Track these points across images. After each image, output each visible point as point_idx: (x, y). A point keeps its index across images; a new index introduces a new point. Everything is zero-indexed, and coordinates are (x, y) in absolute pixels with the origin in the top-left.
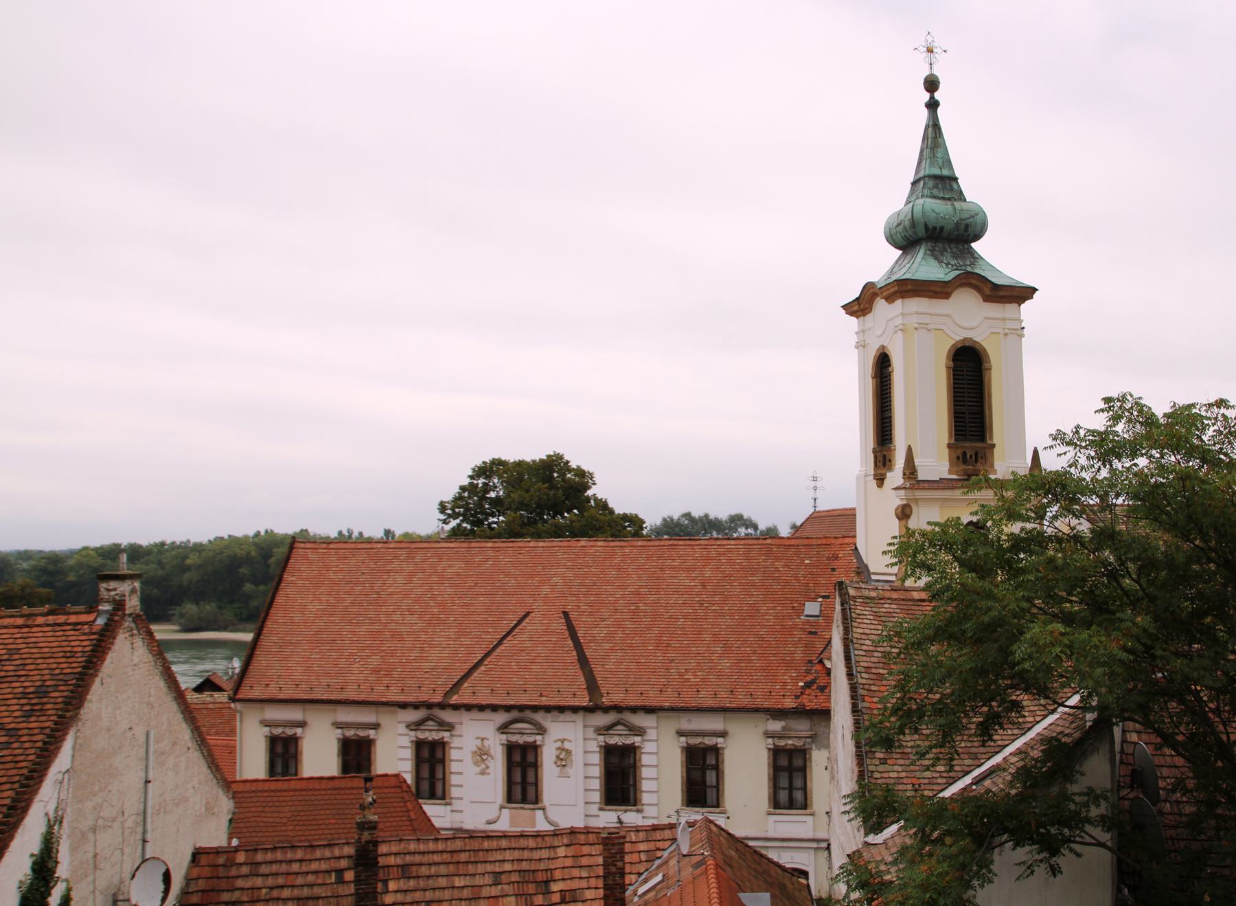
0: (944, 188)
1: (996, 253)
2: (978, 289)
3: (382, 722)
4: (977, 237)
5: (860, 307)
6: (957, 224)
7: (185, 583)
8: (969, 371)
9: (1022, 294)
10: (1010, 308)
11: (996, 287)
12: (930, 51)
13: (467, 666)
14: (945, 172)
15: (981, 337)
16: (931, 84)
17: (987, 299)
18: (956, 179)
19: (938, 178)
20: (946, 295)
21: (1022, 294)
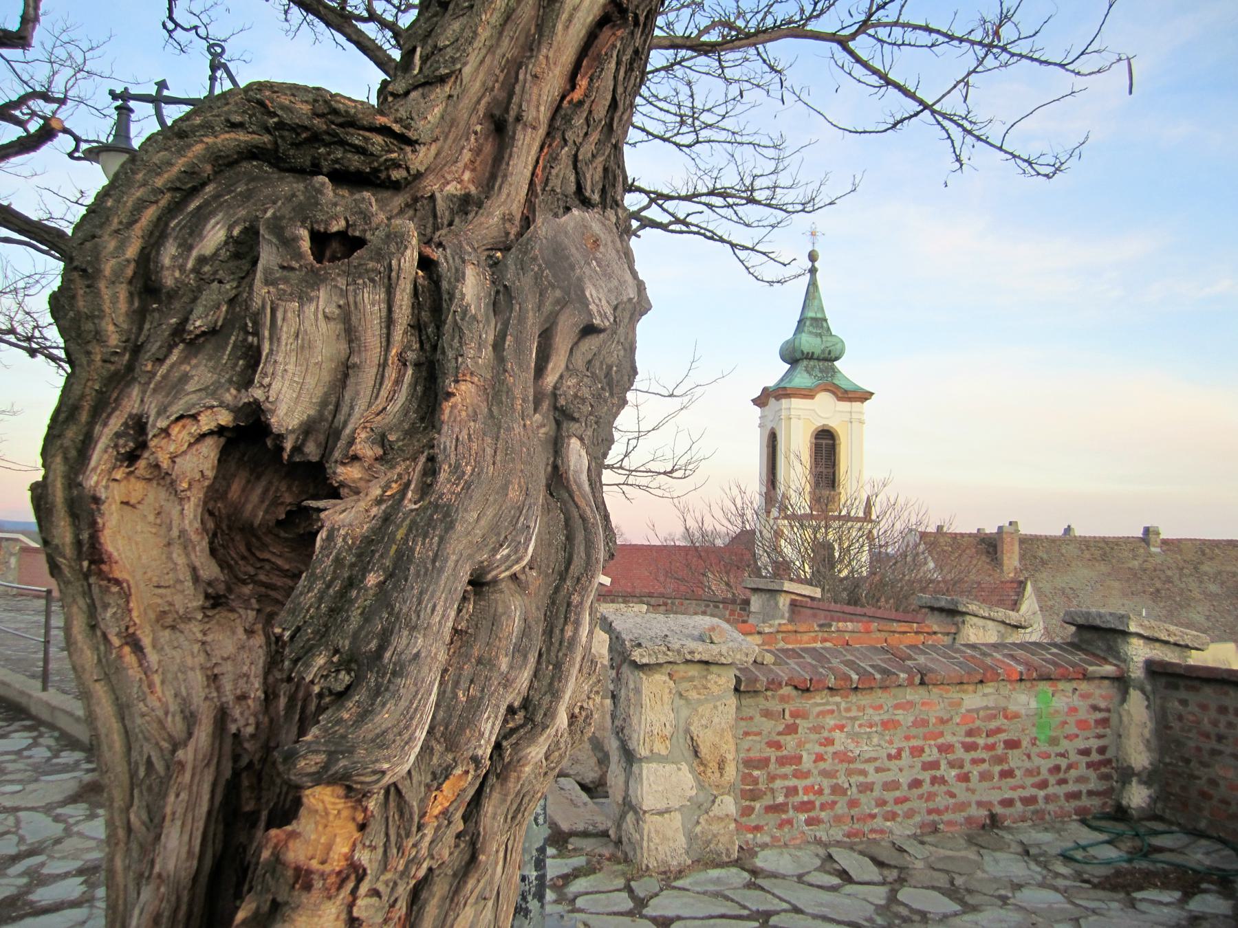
0: (817, 327)
1: (849, 369)
2: (834, 393)
3: (311, 119)
4: (837, 359)
5: (760, 401)
6: (823, 351)
7: (566, 252)
8: (826, 444)
9: (864, 396)
10: (856, 405)
11: (846, 392)
12: (813, 234)
13: (733, 921)
14: (819, 316)
15: (834, 423)
16: (812, 257)
17: (840, 399)
18: (826, 320)
19: (812, 320)
20: (812, 397)
21: (864, 396)
